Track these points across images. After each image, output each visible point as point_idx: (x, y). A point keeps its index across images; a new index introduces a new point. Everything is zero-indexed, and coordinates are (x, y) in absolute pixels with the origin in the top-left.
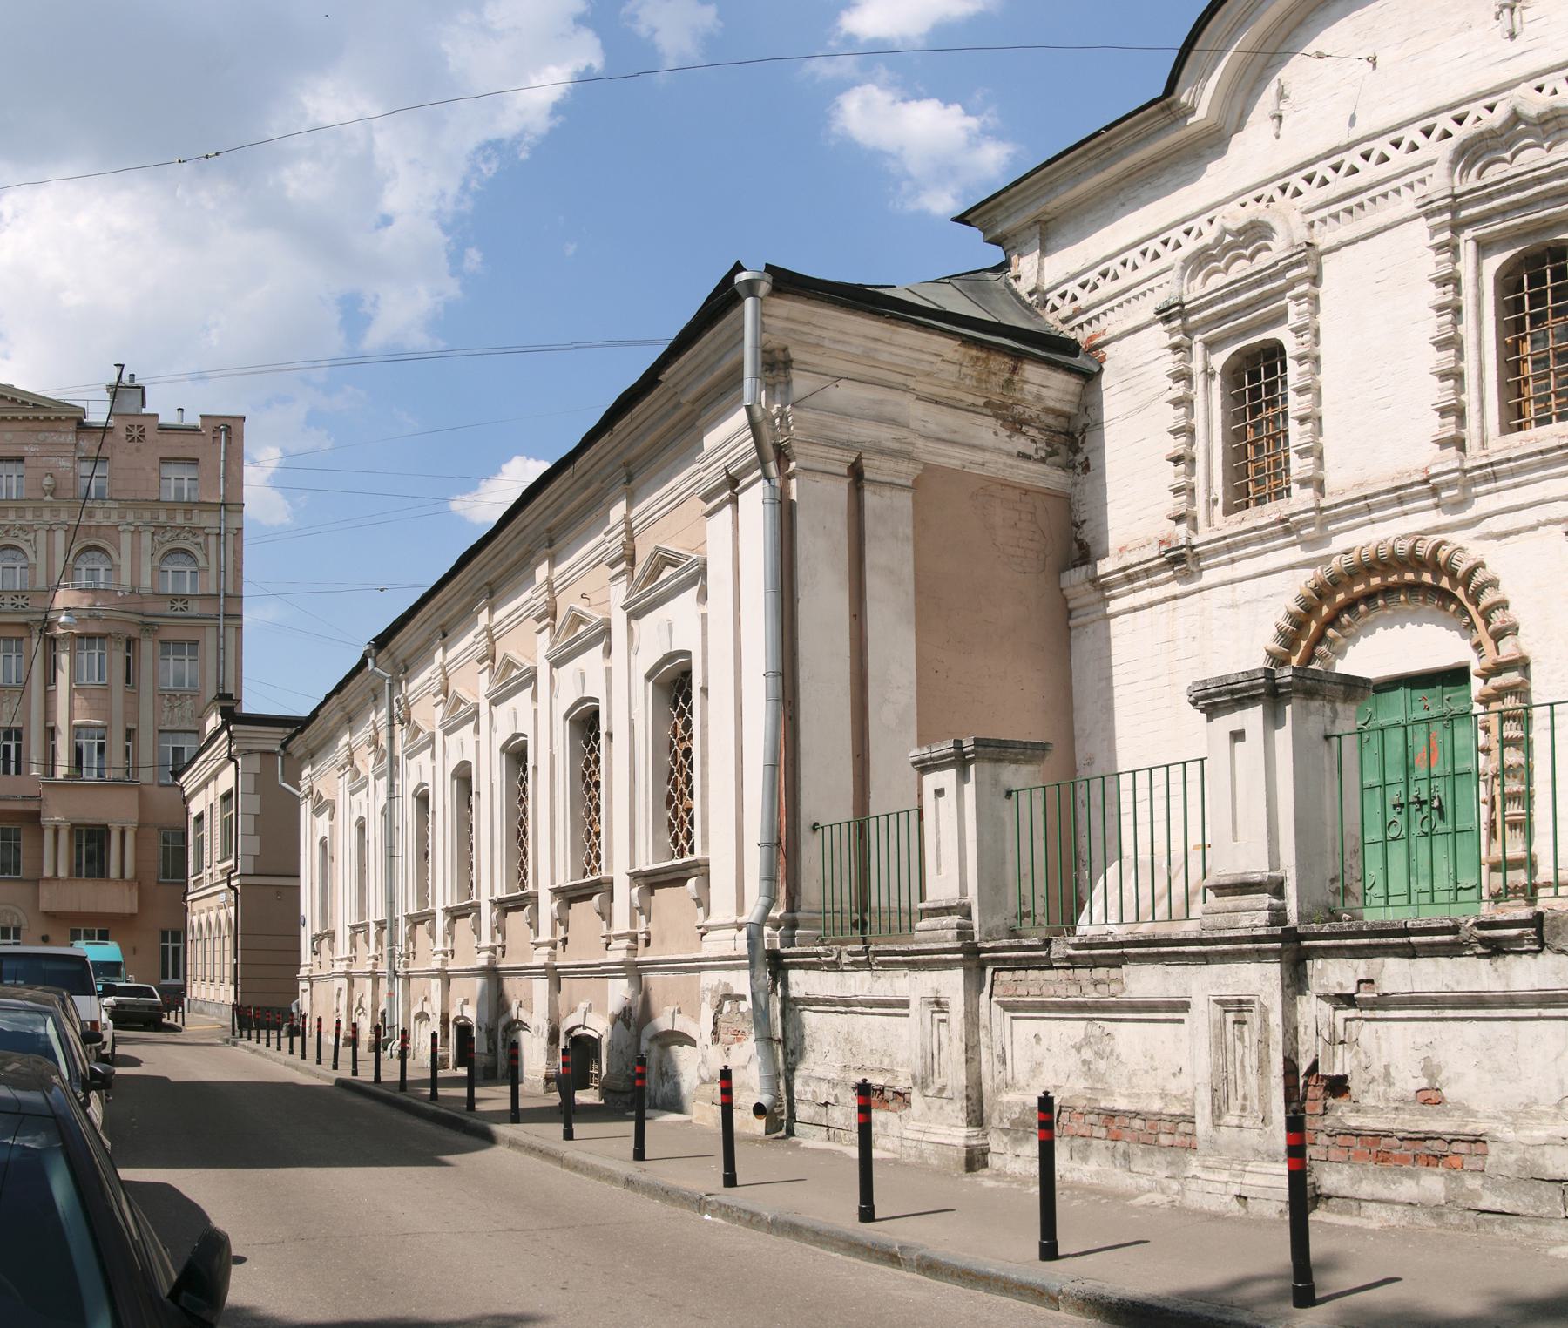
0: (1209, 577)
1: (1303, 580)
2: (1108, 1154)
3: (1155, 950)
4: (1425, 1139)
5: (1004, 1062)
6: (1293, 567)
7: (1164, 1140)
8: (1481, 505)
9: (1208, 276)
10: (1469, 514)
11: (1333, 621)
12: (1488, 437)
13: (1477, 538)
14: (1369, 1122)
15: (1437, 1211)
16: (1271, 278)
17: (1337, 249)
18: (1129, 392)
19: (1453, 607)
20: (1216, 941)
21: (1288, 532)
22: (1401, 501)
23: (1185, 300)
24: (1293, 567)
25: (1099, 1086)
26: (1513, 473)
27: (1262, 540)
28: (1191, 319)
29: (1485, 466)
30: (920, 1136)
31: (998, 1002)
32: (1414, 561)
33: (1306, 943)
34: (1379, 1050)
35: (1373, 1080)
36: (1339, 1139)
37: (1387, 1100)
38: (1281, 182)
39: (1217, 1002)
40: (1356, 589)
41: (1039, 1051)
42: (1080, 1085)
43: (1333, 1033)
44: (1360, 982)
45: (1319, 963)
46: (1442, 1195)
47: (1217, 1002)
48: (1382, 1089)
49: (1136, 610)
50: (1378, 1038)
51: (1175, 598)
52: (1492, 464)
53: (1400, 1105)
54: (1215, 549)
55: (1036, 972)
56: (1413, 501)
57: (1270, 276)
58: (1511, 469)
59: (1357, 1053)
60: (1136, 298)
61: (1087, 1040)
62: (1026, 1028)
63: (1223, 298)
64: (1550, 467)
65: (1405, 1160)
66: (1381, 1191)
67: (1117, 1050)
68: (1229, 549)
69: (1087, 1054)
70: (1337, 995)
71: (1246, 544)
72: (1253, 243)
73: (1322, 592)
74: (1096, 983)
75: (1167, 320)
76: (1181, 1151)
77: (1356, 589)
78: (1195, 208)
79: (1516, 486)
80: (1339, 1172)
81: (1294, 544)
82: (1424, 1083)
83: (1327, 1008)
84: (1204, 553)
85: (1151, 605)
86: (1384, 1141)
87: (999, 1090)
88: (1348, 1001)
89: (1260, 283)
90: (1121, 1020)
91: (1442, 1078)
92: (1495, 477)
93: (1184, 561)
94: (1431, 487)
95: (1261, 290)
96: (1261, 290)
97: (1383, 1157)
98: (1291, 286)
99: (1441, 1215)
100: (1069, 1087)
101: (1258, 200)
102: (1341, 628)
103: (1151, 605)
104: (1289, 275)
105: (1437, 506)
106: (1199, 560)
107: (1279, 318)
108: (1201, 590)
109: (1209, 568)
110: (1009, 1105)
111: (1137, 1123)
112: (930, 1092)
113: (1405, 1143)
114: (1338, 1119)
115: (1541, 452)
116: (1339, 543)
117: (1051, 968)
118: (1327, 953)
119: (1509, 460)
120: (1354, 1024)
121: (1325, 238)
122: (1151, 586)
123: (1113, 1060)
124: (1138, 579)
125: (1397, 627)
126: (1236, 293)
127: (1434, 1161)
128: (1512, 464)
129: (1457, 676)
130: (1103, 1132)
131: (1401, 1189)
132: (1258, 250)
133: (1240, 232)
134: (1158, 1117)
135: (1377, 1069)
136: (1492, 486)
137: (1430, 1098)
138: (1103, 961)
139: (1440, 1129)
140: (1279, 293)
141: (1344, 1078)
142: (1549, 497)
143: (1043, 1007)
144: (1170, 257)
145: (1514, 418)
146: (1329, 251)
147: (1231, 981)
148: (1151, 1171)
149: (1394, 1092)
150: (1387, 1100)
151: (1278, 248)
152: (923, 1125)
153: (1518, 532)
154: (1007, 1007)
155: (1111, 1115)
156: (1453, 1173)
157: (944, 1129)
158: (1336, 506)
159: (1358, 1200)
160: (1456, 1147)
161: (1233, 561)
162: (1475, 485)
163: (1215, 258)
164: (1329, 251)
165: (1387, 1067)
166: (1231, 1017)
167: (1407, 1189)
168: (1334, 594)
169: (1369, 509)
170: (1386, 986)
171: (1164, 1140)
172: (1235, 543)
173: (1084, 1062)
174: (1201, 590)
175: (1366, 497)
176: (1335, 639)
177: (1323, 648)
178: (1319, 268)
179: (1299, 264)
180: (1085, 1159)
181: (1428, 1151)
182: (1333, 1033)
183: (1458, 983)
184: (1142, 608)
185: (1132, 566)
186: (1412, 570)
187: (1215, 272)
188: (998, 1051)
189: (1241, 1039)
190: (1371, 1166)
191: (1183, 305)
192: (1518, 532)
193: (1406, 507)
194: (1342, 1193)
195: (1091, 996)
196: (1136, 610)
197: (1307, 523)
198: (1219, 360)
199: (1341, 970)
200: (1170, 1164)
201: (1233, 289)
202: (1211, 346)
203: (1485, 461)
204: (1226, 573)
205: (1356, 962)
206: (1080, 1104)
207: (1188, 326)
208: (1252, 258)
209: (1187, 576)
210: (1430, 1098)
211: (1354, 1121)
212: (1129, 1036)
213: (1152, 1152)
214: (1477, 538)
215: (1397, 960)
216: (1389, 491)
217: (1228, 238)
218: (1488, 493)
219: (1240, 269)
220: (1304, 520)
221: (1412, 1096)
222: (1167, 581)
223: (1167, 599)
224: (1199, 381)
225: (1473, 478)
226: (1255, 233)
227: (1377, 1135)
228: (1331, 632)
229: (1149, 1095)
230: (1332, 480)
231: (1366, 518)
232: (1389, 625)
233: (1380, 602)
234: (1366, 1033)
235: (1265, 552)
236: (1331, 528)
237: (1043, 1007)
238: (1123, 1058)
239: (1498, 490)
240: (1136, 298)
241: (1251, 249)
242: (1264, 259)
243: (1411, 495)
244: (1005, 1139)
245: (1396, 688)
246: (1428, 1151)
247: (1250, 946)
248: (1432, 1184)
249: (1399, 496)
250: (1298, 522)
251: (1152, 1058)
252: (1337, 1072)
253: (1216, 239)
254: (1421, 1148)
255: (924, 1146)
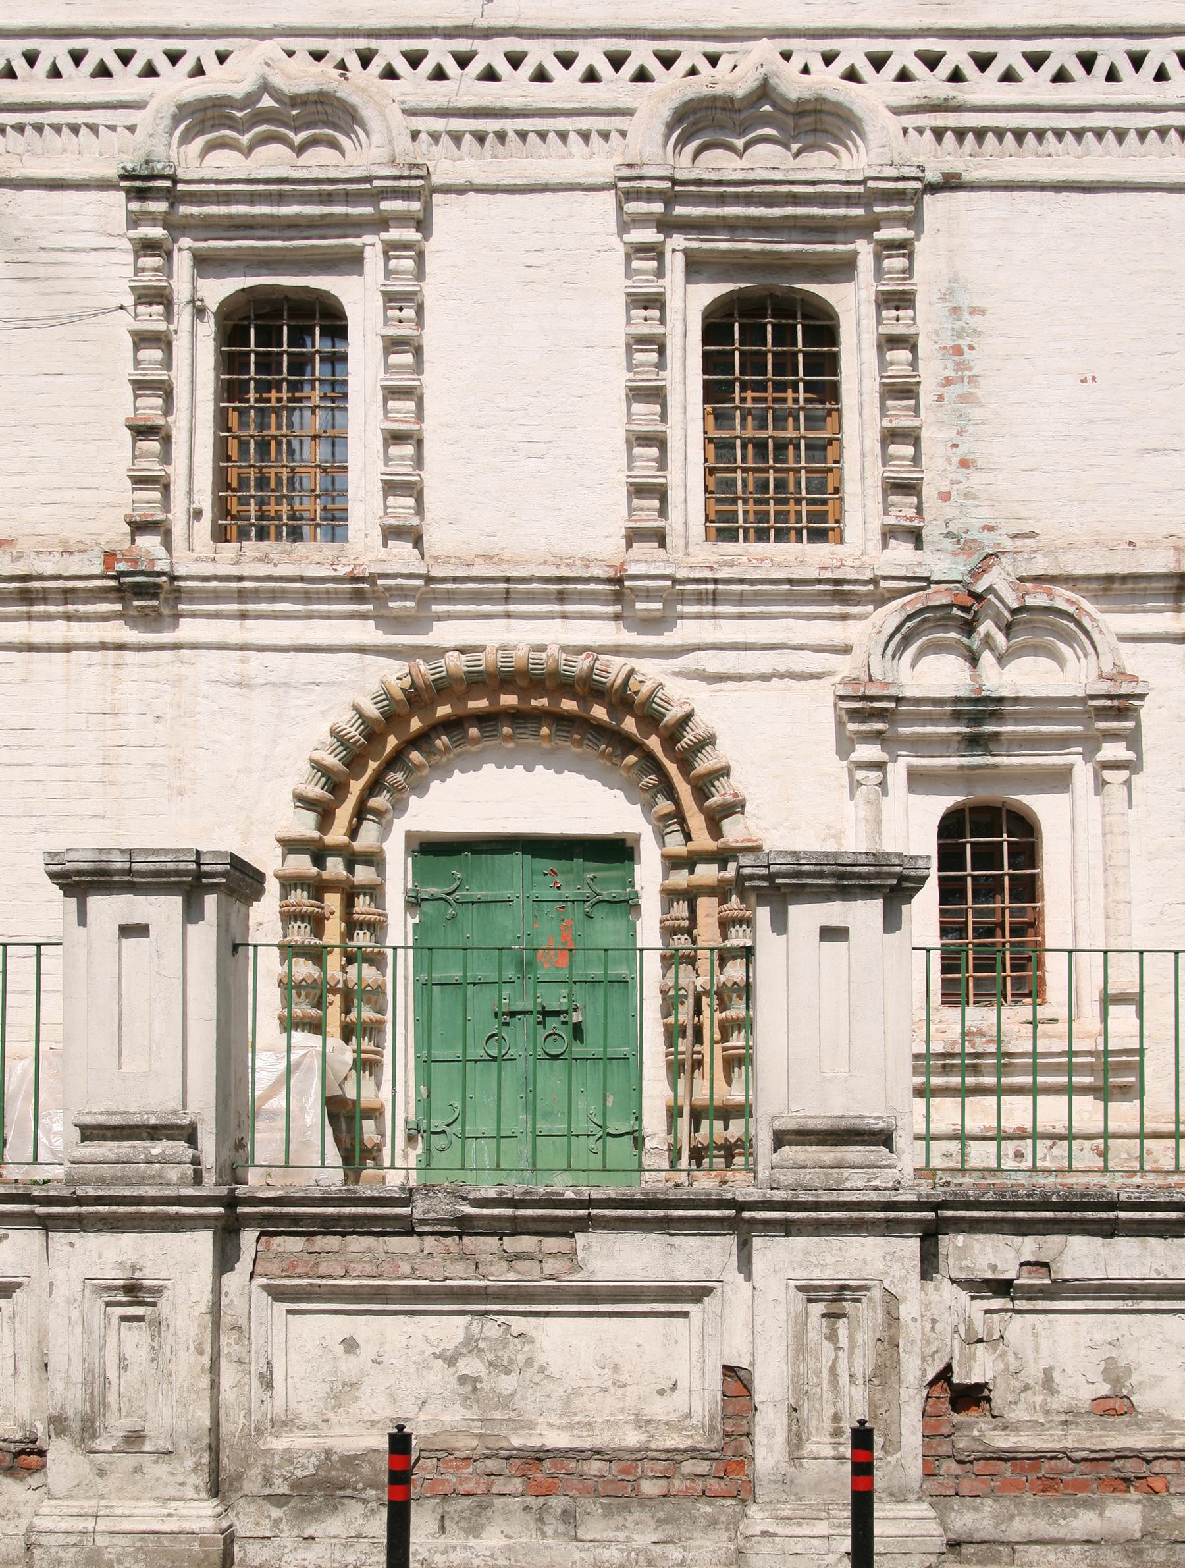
0: (188, 630)
1: (393, 674)
2: (530, 1518)
3: (661, 1213)
4: (1112, 1460)
5: (269, 1385)
6: (361, 650)
7: (649, 1487)
8: (685, 632)
9: (210, 147)
10: (669, 639)
11: (420, 741)
12: (692, 549)
13: (676, 674)
14: (1027, 1441)
15: (1132, 1547)
16: (348, 198)
17: (461, 190)
18: (27, 287)
19: (631, 759)
20: (817, 1206)
21: (358, 596)
22: (561, 597)
23: (181, 174)
24: (361, 650)
25: (497, 1415)
26: (741, 599)
27: (307, 598)
28: (184, 210)
29: (706, 581)
30: (89, 1524)
31: (266, 1288)
32: (590, 688)
33: (949, 1213)
34: (1036, 1350)
35: (1026, 1388)
36: (978, 1467)
37: (1047, 1412)
38: (363, 43)
39: (799, 1288)
40: (534, 703)
41: (349, 1366)
42: (454, 1415)
43: (970, 1329)
44: (1022, 1265)
45: (960, 1239)
46: (1137, 1527)
47: (799, 1288)
48: (1039, 1399)
49: (31, 648)
50: (1035, 1335)
51: (121, 647)
52: (716, 581)
53: (1070, 1418)
54: (215, 591)
55: (370, 1240)
56: (581, 601)
57: (347, 193)
58: (742, 593)
59: (1003, 1354)
60: (57, 129)
61: (471, 1345)
62: (322, 1329)
63: (252, 198)
64: (796, 602)
65: (1083, 1486)
66: (1042, 1527)
67: (541, 1359)
68: (242, 596)
69: (471, 1366)
70: (986, 1281)
71: (274, 596)
72: (308, 126)
73: (418, 697)
74: (512, 1258)
75: (141, 194)
76: (687, 1503)
77: (534, 703)
78: (198, 21)
79: (742, 617)
80: (976, 1509)
81: (364, 616)
82: (1105, 1389)
83: (964, 1296)
84: (191, 591)
85: (67, 648)
86: (1046, 1465)
87: (260, 1431)
88: (1002, 1288)
89: (327, 198)
90: (548, 1314)
91: (1135, 1379)
92: (714, 598)
93: (155, 596)
94: (619, 589)
95: (327, 210)
96: (327, 210)
97: (1049, 1484)
98: (382, 223)
99: (1139, 1552)
100: (437, 1418)
101: (318, 56)
102: (429, 752)
103: (67, 648)
104: (386, 205)
105: (617, 617)
106: (178, 600)
107: (352, 262)
108: (177, 647)
109: (194, 615)
110: (288, 1457)
111: (595, 1467)
112: (102, 1444)
113: (1083, 1466)
114: (975, 1439)
115: (790, 581)
116: (444, 634)
117: (410, 1232)
118: (974, 1227)
119: (741, 581)
120: (996, 1317)
121: (446, 166)
122: (68, 617)
123: (531, 1374)
124: (45, 600)
125: (519, 768)
126: (280, 198)
127: (1123, 1486)
128: (745, 587)
129: (616, 851)
130: (517, 1484)
131: (1075, 1523)
132: (313, 142)
133: (296, 101)
134: (642, 1454)
135: (1033, 1372)
136: (708, 609)
137: (1115, 1406)
138: (533, 1227)
139: (1139, 1445)
140: (358, 226)
141: (981, 1386)
142: (794, 642)
143: (416, 1295)
144: (175, 86)
145: (723, 528)
146: (447, 190)
147: (829, 1259)
148: (622, 1536)
149: (1055, 1403)
150: (1047, 1412)
151: (359, 158)
152: (89, 1505)
153: (740, 678)
154: (278, 1294)
155: (537, 1457)
156: (1156, 1498)
157: (147, 1507)
158: (455, 580)
159: (1011, 1544)
160: (1157, 1467)
161: (243, 616)
162: (682, 602)
163: (241, 127)
164: (447, 190)
165: (1048, 1372)
166: (818, 1308)
167: (1085, 1522)
168: (433, 704)
169: (507, 597)
170: (1068, 1270)
171: (649, 1487)
172: (256, 591)
173: (463, 1379)
174: (177, 647)
175: (508, 580)
176: (419, 767)
177: (397, 777)
178: (428, 208)
179: (407, 194)
180: (475, 1530)
181: (1118, 1473)
182: (970, 1329)
183: (1174, 1268)
184: (50, 648)
185: (40, 578)
186: (574, 696)
187: (222, 144)
188: (258, 1367)
189: (832, 1337)
190: (1029, 1497)
191: (175, 180)
192: (740, 678)
193: (569, 608)
194: (977, 1537)
195: (502, 1277)
196: (31, 648)
197: (402, 593)
198: (218, 290)
199: (995, 1249)
200: (661, 1522)
201: (277, 190)
202: (204, 263)
203: (707, 574)
204: (230, 631)
205: (1018, 1240)
206: (466, 1445)
207: (173, 219)
208: (300, 149)
209: (149, 620)
210: (1115, 1406)
211: (1003, 1441)
212: (562, 1340)
213: (627, 1508)
214: (676, 674)
215: (1086, 1239)
216: (547, 580)
217: (267, 102)
218: (699, 616)
219: (273, 161)
220: (401, 588)
221: (1087, 1405)
222: (105, 618)
223: (103, 646)
224: (183, 316)
225: (682, 593)
226: (323, 115)
227: (1039, 1457)
228: (415, 756)
229: (612, 1424)
230: (436, 537)
231: (500, 608)
232: (505, 761)
233: (545, 730)
234: (1018, 1328)
235: (309, 616)
236: (434, 608)
237: (336, 1294)
238: (553, 1370)
239: (714, 616)
240: (57, 129)
241: (304, 135)
242: (320, 162)
243: (581, 592)
244: (276, 1513)
245: (509, 851)
246: (1118, 1473)
247: (881, 1215)
248: (1125, 1514)
249: (562, 591)
250: (388, 589)
251: (616, 1368)
252: (975, 1379)
253: (249, 95)
254: (1108, 1470)
255: (101, 1541)
